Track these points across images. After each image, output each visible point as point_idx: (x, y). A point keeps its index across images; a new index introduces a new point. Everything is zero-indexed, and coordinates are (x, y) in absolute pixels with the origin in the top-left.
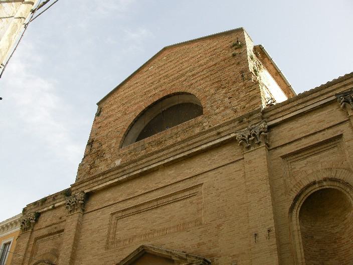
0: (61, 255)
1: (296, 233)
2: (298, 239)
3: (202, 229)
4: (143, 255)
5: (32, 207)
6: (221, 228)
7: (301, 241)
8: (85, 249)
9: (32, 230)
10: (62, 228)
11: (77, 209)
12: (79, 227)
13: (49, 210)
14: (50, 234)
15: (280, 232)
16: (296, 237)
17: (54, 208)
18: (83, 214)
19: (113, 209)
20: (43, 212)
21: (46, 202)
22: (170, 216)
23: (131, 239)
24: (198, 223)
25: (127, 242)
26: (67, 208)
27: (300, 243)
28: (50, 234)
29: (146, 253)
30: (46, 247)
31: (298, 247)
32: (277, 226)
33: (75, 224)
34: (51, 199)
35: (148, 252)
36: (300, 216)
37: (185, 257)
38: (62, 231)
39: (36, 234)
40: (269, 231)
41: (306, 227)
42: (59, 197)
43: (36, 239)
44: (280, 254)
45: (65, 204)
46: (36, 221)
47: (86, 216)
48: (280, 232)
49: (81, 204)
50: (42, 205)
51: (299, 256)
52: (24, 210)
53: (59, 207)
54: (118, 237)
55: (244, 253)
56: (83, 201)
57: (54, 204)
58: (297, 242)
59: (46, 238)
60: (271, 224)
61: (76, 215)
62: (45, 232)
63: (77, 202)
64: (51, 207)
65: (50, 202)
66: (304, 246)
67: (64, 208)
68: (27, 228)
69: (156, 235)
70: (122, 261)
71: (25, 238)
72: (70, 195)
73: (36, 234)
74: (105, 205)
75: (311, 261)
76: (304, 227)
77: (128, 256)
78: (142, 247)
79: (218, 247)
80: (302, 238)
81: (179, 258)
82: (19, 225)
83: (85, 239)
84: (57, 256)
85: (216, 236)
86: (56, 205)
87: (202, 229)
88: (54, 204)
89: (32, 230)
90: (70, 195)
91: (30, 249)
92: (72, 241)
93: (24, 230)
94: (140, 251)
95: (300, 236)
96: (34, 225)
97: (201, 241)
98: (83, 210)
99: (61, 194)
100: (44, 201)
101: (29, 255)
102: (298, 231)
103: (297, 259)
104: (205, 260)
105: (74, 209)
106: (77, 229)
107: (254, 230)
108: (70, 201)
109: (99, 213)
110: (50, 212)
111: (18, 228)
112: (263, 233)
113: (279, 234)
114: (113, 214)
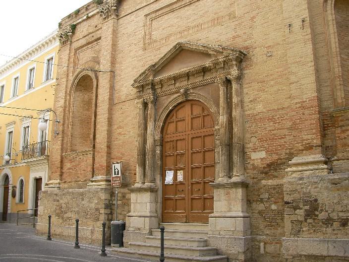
0: (101, 61)
1: (331, 23)
2: (332, 29)
3: (237, 23)
4: (180, 52)
5: (67, 20)
6: (255, 20)
7: (336, 30)
8: (124, 53)
9: (71, 42)
10: (99, 36)
11: (111, 15)
12: (115, 32)
13: (84, 21)
14: (89, 43)
15: (314, 22)
16: (331, 27)
17: (88, 18)
18: (118, 20)
19: (147, 11)
20: (78, 24)
21: (80, 13)
22: (203, 12)
23: (168, 37)
24: (232, 16)
25: (164, 41)
26: (101, 15)
27: (335, 43)
28: (89, 43)
29: (183, 50)
30: (86, 56)
31: (332, 36)
32: (311, 17)
33: (111, 30)
34: (84, 10)
35: (184, 48)
36: (335, 5)
37: (221, 50)
38: (99, 38)
39: (76, 45)
40: (303, 21)
41: (341, 17)
42: (92, 6)
43: (76, 50)
44: (314, 44)
45: (98, 12)
46: (73, 33)
47: (121, 21)
48: (314, 22)
49: (115, 10)
50: (76, 17)
51: (333, 46)
52: (60, 25)
53: (93, 16)
54: (154, 37)
55: (278, 44)
56: (116, 6)
57: (88, 14)
58: (332, 31)
59: (85, 48)
60: (306, 14)
61: (110, 22)
62: (83, 42)
63: (110, 8)
64: (85, 17)
65: (83, 13)
66: (339, 35)
67: (97, 16)
68: (65, 41)
69: (191, 32)
70: (161, 59)
71: (65, 50)
72: (102, 3)
73: (76, 45)
74: (138, 8)
75: (345, 50)
76: (339, 17)
77: (166, 54)
78: (179, 44)
79: (253, 38)
80: (337, 28)
81: (215, 52)
82: (58, 39)
83: (122, 43)
84: (99, 63)
85: (250, 28)
86: (90, 15)
87: (237, 23)
88: (88, 14)
89: (71, 42)
90: (102, 3)
91: (72, 60)
92: (110, 47)
93: (64, 43)
94: (177, 48)
95: (335, 25)
96: (72, 36)
97: (235, 34)
98: (117, 16)
99: (93, 3)
100: (78, 12)
101: (72, 65)
102: (333, 20)
103: (331, 48)
104: (240, 52)
105: (108, 17)
106: (113, 34)
107: (288, 21)
108: (103, 9)
109: (132, 17)
110: (85, 23)
111: (57, 43)
112: (297, 24)
113: (313, 23)
114: (146, 16)
